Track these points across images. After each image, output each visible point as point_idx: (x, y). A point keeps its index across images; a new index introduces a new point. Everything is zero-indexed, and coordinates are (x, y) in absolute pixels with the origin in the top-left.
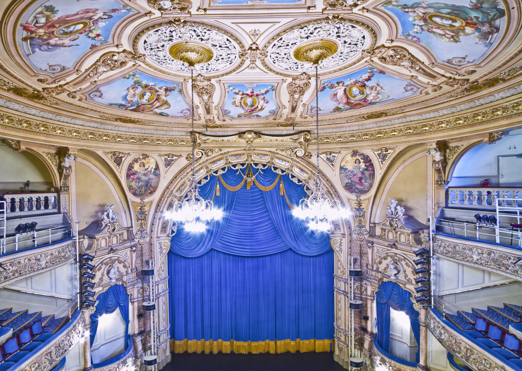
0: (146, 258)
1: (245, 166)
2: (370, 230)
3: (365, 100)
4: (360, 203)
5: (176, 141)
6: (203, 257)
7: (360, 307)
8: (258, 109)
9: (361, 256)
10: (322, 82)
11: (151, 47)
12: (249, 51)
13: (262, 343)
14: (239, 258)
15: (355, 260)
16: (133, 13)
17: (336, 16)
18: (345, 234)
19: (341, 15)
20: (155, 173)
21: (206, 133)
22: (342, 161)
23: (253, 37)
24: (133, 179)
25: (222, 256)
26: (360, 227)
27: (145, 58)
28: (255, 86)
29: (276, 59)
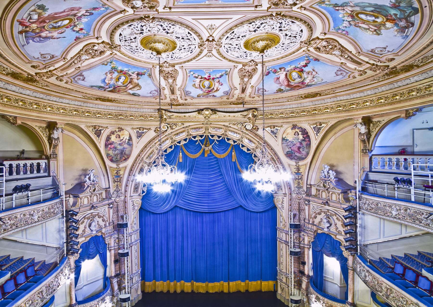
0: (121, 213)
1: (203, 137)
2: (307, 191)
3: (303, 83)
4: (298, 168)
5: (146, 117)
6: (168, 213)
7: (298, 254)
8: (214, 90)
9: (299, 212)
10: (267, 68)
11: (125, 39)
12: (207, 42)
15: (295, 215)
16: (110, 11)
17: (279, 13)
18: (286, 194)
19: (283, 12)
20: (129, 143)
21: (171, 110)
22: (283, 133)
23: (210, 31)
24: (111, 148)
25: (184, 212)
26: (299, 188)
27: (120, 48)
28: (212, 71)
29: (229, 49)
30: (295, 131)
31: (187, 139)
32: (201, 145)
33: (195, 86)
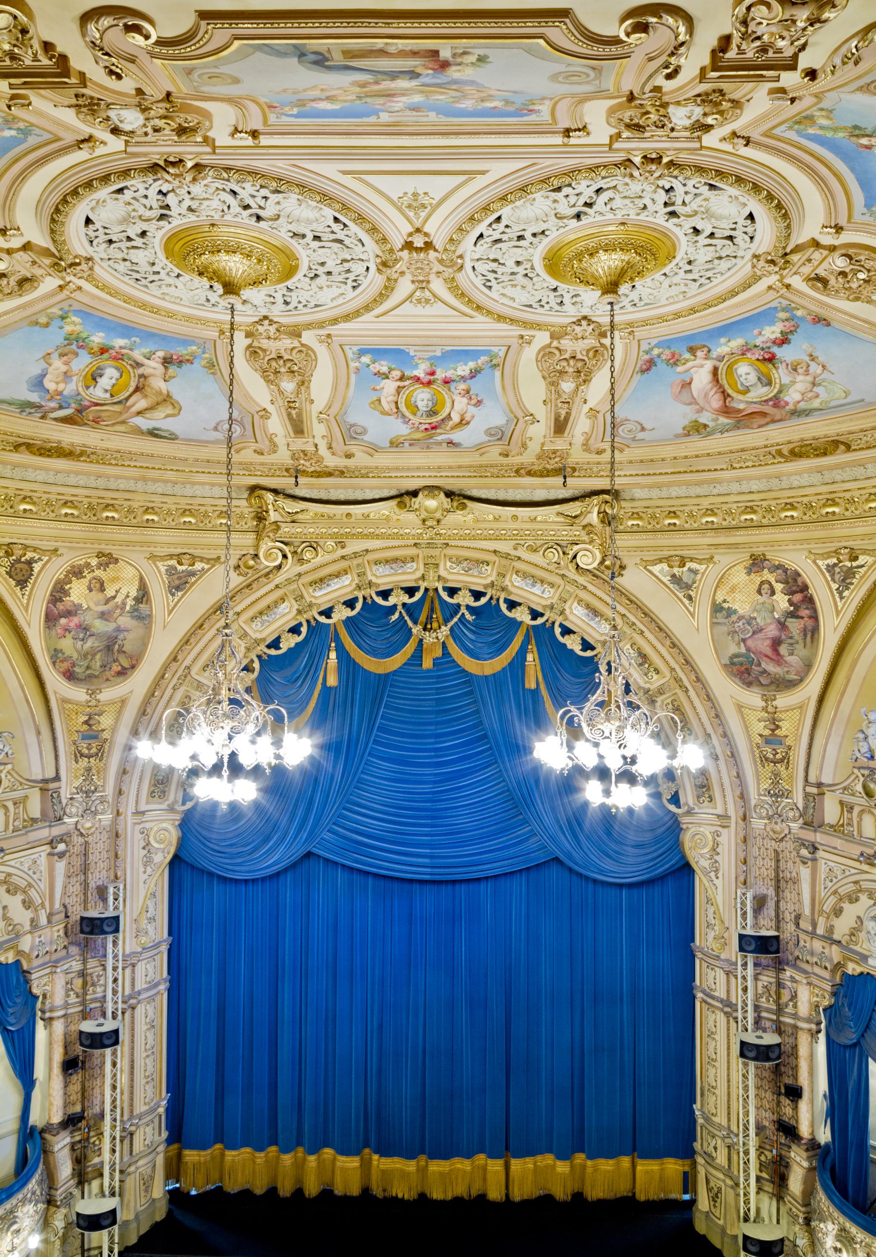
0: (96, 878)
1: (418, 596)
2: (806, 807)
3: (776, 401)
4: (774, 719)
5: (206, 515)
6: (282, 878)
7: (773, 1055)
8: (451, 423)
9: (777, 888)
10: (645, 346)
11: (108, 237)
12: (405, 254)
13: (461, 1165)
14: (396, 885)
15: (760, 903)
16: (40, 139)
17: (654, 156)
18: (728, 817)
19: (669, 153)
20: (136, 610)
21: (299, 492)
22: (717, 586)
23: (411, 214)
25: (341, 876)
26: (776, 795)
27: (91, 269)
29: (491, 276)
30: (758, 580)
31: (356, 599)
32: (410, 623)
33: (379, 408)
